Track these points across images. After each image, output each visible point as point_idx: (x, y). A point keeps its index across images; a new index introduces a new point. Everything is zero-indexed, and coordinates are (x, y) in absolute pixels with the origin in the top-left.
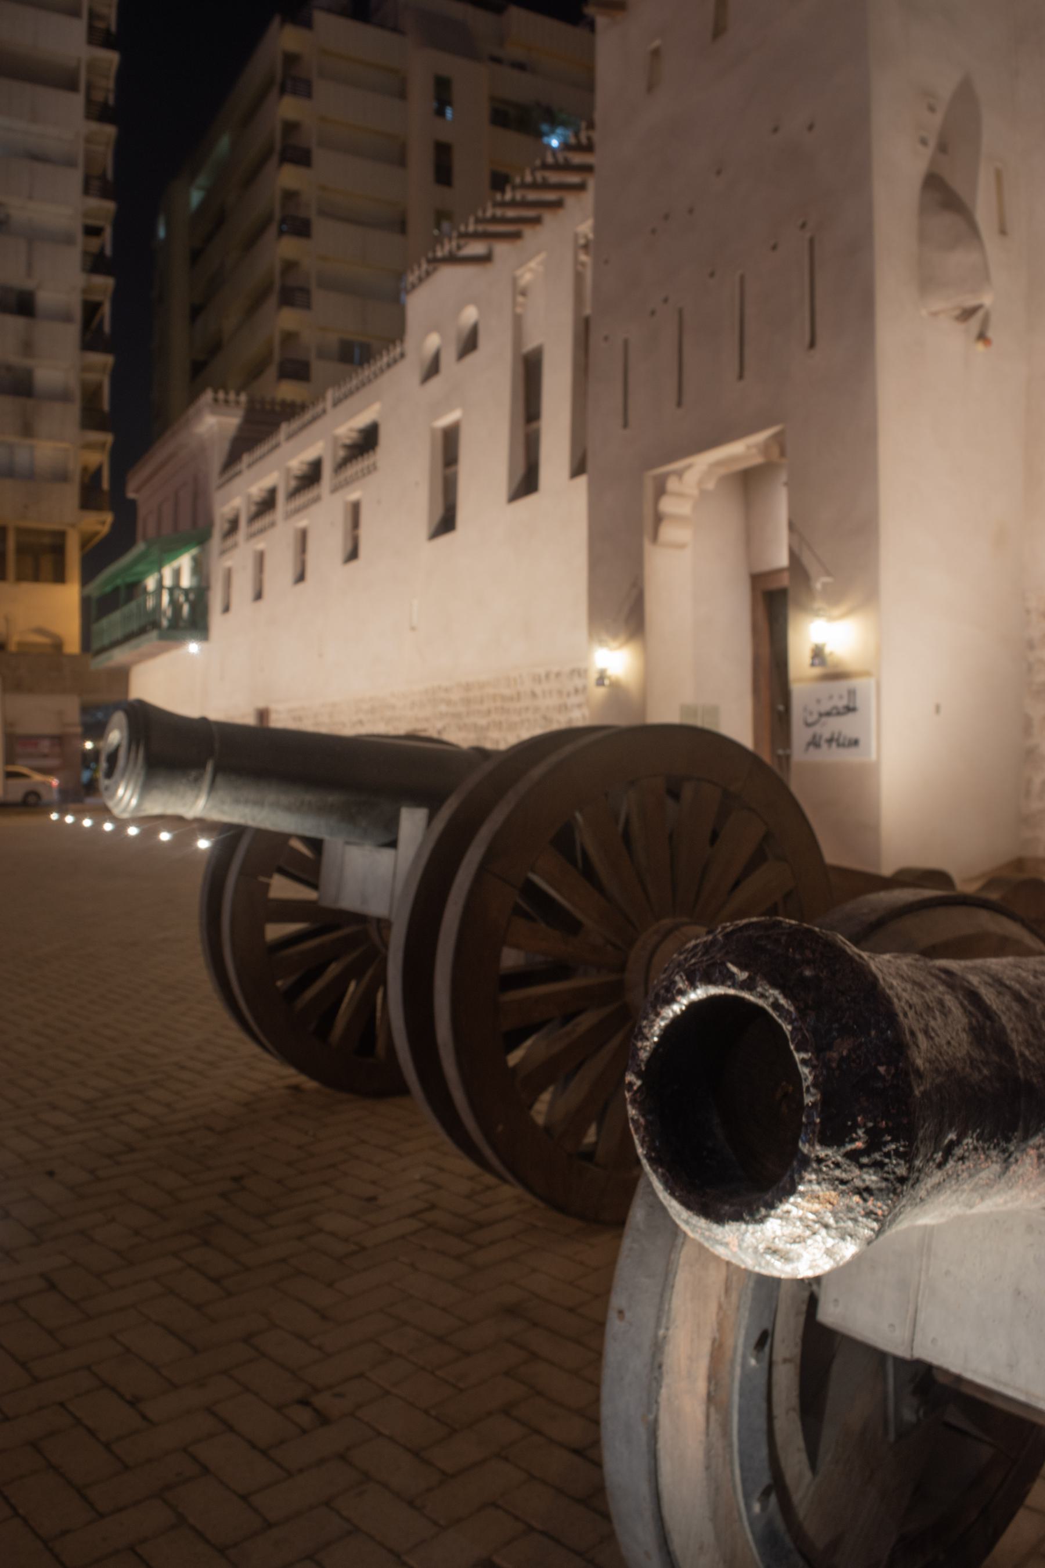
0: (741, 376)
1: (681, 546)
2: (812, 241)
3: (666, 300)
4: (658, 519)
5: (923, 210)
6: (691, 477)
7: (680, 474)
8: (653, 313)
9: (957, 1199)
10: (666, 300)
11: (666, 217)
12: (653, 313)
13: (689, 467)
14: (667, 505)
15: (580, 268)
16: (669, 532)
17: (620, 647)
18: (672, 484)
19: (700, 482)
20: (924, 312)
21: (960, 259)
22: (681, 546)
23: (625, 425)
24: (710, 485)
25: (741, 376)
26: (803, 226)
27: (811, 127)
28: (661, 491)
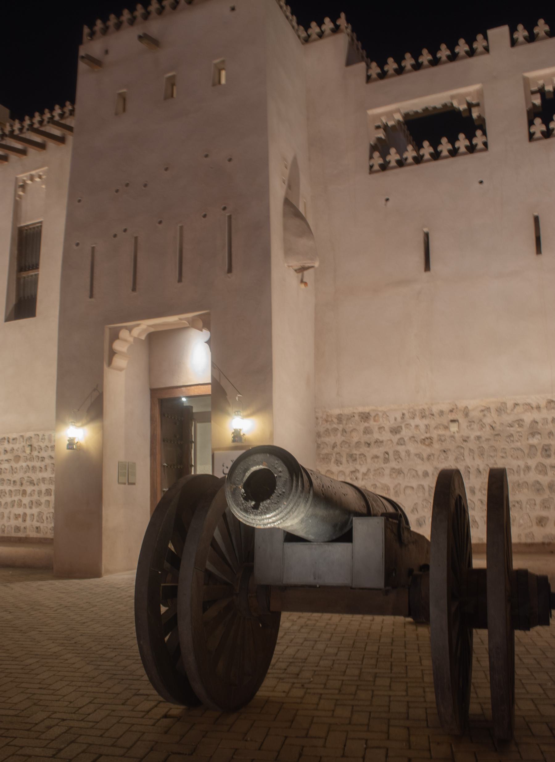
0: (180, 280)
1: (121, 370)
2: (230, 217)
3: (125, 230)
4: (113, 353)
5: (285, 215)
6: (136, 332)
7: (130, 329)
8: (115, 236)
9: (148, 684)
10: (125, 230)
11: (127, 185)
12: (115, 236)
13: (138, 325)
14: (118, 346)
15: (18, 198)
16: (118, 361)
17: (83, 425)
18: (124, 334)
19: (140, 334)
20: (286, 265)
21: (303, 243)
22: (121, 370)
23: (91, 296)
24: (143, 337)
25: (180, 280)
26: (224, 209)
27: (230, 160)
28: (115, 336)
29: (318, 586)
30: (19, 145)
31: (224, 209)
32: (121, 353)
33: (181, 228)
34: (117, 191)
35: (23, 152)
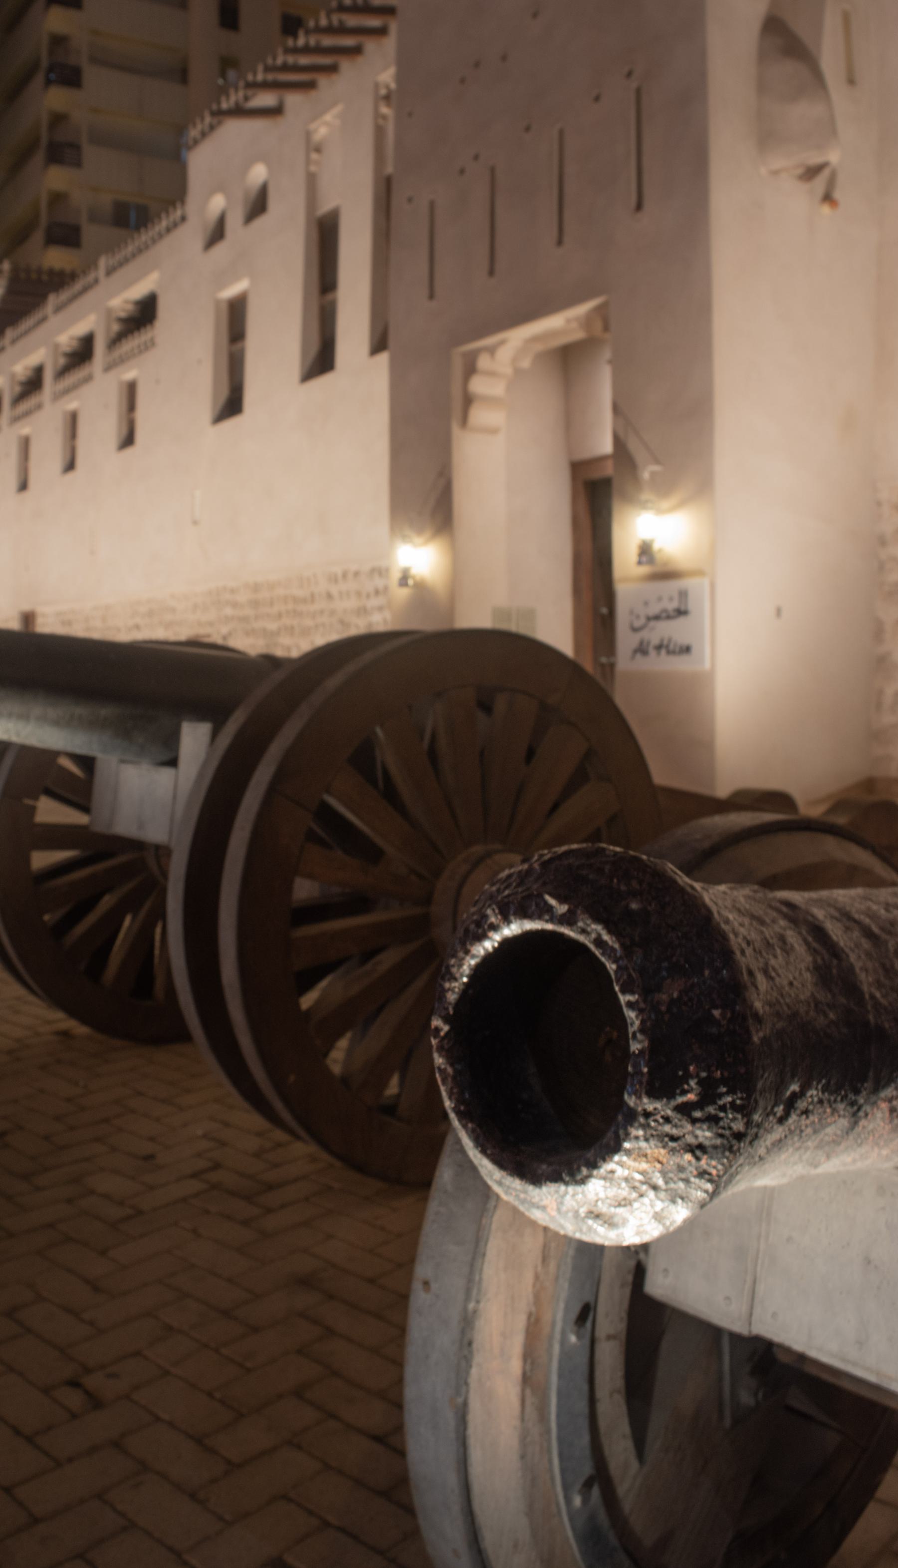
0: (560, 242)
1: (494, 431)
2: (638, 91)
3: (476, 157)
4: (468, 401)
6: (505, 354)
8: (462, 171)
10: (476, 157)
11: (477, 65)
12: (462, 171)
13: (503, 342)
14: (478, 385)
16: (480, 415)
17: (426, 543)
18: (483, 362)
19: (515, 360)
22: (494, 431)
23: (431, 296)
24: (526, 363)
25: (560, 242)
26: (629, 74)
28: (470, 369)
29: (637, 1052)
30: (349, 41)
31: (629, 74)
32: (491, 401)
33: (561, 133)
34: (463, 81)
35: (357, 51)
